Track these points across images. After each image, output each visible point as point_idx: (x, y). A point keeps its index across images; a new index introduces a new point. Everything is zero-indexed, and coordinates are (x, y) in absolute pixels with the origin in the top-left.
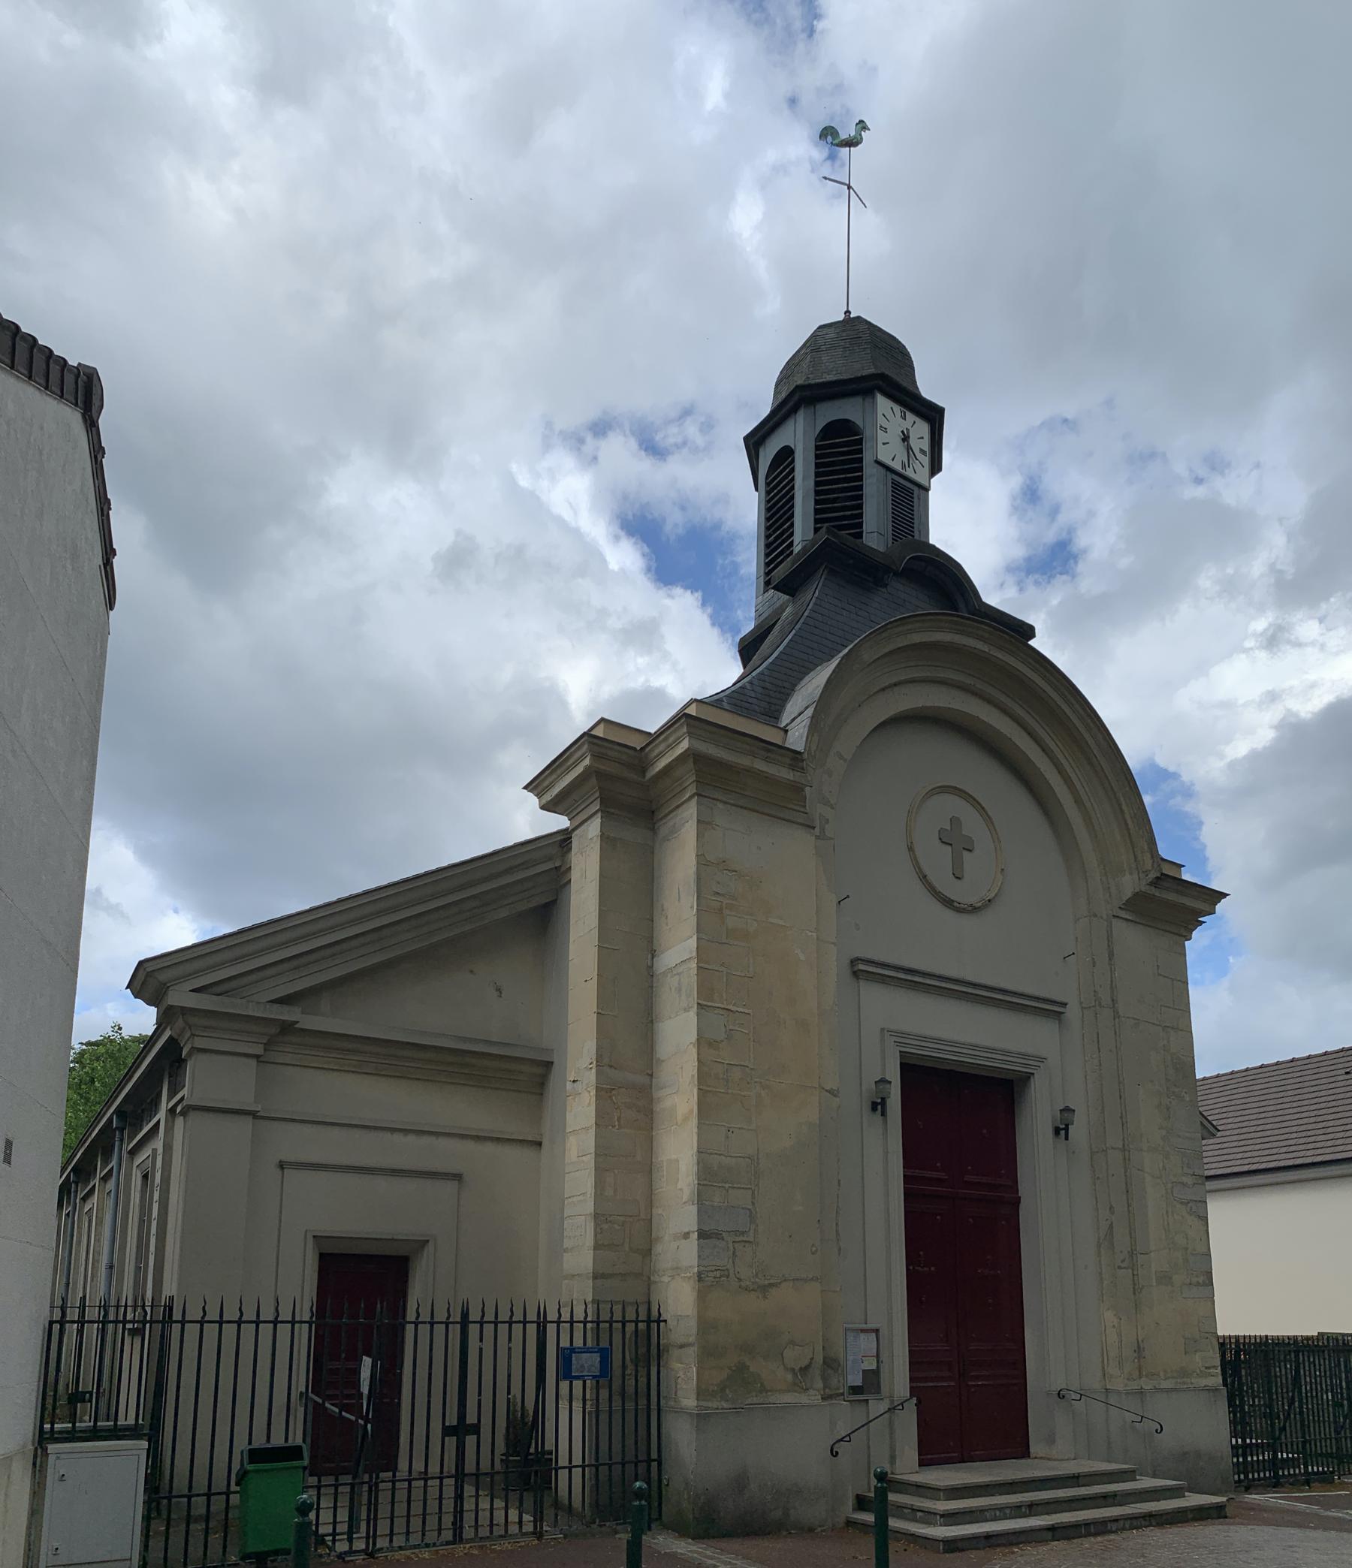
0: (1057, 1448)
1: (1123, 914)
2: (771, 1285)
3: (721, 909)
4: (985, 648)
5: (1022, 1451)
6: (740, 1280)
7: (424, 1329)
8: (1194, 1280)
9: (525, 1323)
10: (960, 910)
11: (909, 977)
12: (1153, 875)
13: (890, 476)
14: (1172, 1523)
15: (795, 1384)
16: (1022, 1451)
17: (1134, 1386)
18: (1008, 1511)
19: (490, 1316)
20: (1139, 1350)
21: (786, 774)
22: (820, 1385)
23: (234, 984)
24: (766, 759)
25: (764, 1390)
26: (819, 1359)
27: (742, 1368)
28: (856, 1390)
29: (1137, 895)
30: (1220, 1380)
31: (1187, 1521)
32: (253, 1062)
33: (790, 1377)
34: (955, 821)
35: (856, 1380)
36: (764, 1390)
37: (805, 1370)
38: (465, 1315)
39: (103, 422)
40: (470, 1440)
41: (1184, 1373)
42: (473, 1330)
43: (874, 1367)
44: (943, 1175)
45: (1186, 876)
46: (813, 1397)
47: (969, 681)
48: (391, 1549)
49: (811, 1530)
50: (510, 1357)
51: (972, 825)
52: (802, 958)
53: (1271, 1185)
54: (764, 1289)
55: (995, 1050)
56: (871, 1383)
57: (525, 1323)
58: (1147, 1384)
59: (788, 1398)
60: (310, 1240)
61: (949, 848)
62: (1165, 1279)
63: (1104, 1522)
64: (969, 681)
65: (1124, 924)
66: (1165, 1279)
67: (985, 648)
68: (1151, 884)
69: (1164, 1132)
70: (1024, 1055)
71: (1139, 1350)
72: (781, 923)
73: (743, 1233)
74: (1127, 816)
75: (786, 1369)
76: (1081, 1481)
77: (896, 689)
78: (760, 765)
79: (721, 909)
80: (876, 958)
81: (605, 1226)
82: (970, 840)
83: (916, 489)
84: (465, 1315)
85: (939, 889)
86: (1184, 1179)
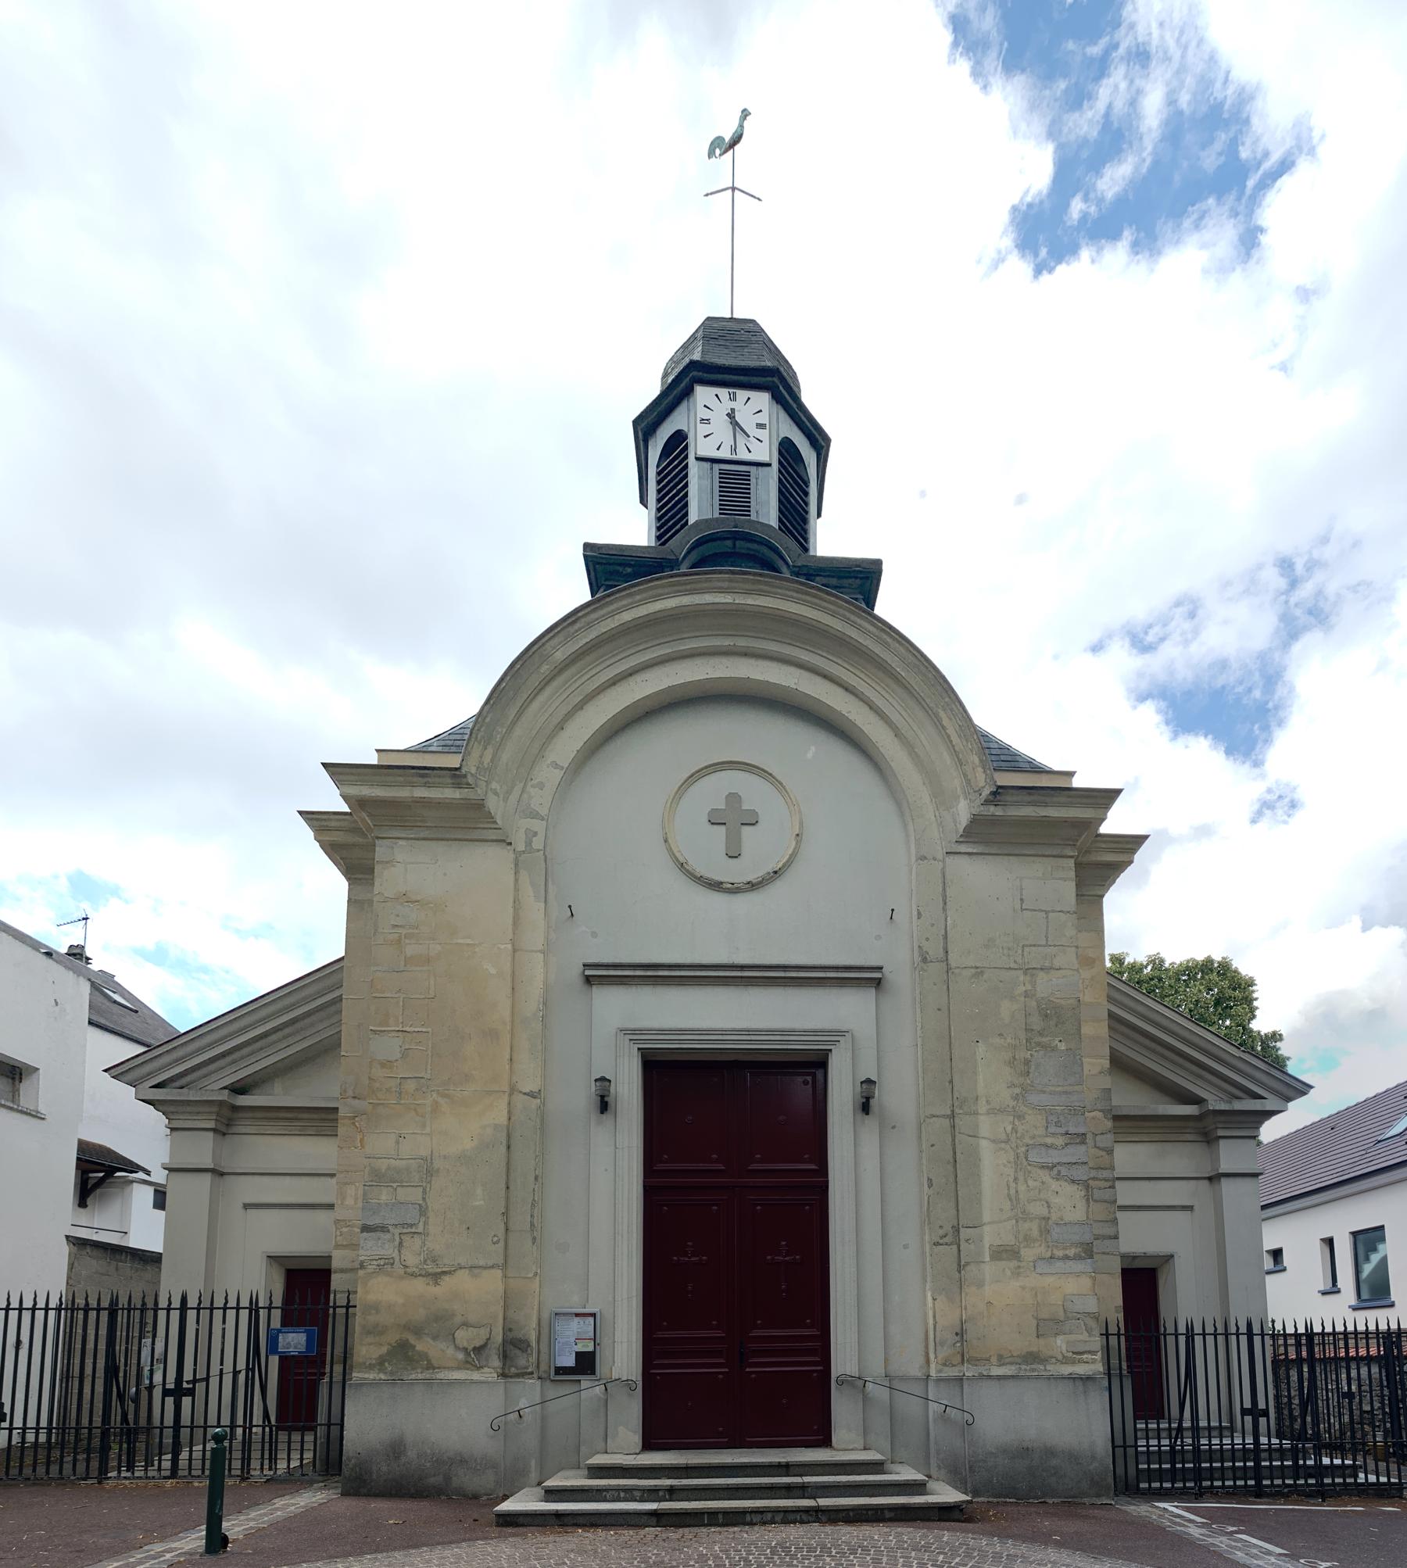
0: (850, 1437)
1: (963, 848)
2: (444, 1273)
3: (399, 941)
4: (727, 599)
5: (826, 1442)
8: (1060, 1253)
9: (238, 1308)
12: (986, 792)
13: (717, 467)
16: (826, 1442)
17: (952, 1372)
19: (232, 1303)
20: (961, 1334)
21: (450, 794)
23: (188, 1079)
24: (426, 785)
25: (430, 1367)
28: (560, 1371)
29: (975, 821)
30: (1100, 1367)
31: (929, 1520)
32: (211, 1134)
33: (461, 1356)
34: (733, 799)
37: (478, 1350)
38: (184, 1300)
39: (1056, 769)
40: (186, 1401)
41: (1032, 1358)
42: (191, 1315)
43: (590, 1349)
45: (1077, 782)
46: (489, 1374)
47: (727, 642)
48: (119, 1477)
49: (475, 1497)
50: (223, 1337)
51: (753, 792)
52: (493, 971)
54: (436, 1277)
56: (586, 1363)
58: (969, 1371)
61: (723, 828)
62: (1002, 1253)
64: (727, 642)
65: (965, 860)
66: (1002, 1253)
67: (727, 599)
68: (987, 802)
69: (1018, 1090)
71: (961, 1334)
72: (469, 941)
73: (411, 1226)
74: (951, 731)
75: (457, 1348)
77: (631, 679)
79: (399, 941)
80: (617, 961)
81: (345, 1230)
82: (754, 813)
83: (753, 469)
84: (184, 1300)
85: (707, 874)
86: (1049, 1141)
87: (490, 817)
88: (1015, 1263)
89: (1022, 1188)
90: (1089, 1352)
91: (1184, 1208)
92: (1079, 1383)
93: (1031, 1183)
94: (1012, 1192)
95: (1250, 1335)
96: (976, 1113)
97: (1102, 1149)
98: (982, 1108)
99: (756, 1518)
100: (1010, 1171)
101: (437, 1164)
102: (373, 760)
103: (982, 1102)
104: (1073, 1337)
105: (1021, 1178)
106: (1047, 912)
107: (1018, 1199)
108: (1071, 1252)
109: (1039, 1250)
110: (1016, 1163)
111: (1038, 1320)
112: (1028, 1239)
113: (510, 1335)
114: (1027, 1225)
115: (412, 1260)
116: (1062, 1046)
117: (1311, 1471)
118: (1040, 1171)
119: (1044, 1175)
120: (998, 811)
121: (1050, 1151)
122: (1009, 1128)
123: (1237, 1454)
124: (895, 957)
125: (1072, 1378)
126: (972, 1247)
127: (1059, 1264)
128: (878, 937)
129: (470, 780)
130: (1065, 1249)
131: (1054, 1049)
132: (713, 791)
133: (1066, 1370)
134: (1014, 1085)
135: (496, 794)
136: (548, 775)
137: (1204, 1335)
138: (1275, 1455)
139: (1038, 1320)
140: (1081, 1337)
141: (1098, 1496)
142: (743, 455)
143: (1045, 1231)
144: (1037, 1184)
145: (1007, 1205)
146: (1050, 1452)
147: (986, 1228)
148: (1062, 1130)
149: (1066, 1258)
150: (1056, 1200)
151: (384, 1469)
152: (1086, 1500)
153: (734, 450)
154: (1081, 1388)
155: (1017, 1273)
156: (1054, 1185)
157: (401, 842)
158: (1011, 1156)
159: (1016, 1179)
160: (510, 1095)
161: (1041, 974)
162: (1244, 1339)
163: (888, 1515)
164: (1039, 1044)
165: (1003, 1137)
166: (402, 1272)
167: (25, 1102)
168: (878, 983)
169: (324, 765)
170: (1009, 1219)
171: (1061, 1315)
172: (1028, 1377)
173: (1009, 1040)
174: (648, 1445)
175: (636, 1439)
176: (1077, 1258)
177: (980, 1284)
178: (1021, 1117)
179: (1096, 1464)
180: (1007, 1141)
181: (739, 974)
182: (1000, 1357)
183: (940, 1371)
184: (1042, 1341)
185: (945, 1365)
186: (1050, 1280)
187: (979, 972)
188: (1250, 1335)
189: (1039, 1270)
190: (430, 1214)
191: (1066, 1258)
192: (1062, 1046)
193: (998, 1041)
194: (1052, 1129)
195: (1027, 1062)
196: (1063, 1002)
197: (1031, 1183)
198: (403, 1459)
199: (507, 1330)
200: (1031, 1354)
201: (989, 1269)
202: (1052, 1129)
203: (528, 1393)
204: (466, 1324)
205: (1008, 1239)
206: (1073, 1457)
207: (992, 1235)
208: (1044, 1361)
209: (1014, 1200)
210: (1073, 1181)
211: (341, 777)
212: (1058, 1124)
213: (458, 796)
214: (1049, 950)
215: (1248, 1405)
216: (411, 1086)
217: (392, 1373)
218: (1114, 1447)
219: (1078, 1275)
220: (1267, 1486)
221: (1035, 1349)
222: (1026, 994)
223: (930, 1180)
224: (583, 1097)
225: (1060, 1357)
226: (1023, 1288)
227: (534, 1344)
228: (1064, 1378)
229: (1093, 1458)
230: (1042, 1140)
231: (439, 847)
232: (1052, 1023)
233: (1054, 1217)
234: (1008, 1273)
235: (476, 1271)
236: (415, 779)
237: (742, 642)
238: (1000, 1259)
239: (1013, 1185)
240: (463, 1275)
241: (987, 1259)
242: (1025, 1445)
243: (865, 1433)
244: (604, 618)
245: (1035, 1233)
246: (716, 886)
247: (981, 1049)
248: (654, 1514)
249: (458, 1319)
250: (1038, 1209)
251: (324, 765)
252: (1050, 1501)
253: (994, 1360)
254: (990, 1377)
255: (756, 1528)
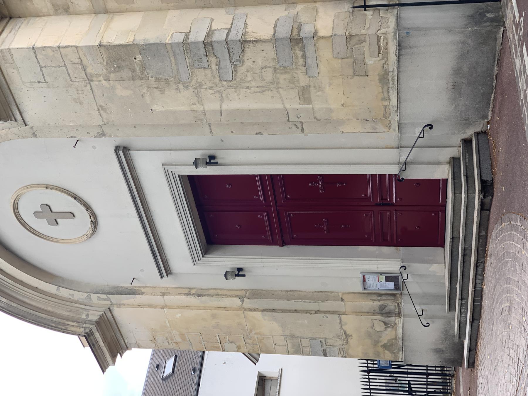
1: (19, 117)
6: (343, 344)
8: (301, 61)
11: (158, 254)
15: (393, 327)
21: (97, 335)
24: (97, 342)
25: (396, 339)
26: (380, 318)
27: (385, 346)
28: (397, 287)
33: (389, 329)
35: (391, 285)
36: (396, 339)
37: (385, 324)
41: (384, 79)
44: (265, 214)
46: (399, 322)
52: (180, 315)
53: (232, 290)
54: (347, 336)
55: (176, 204)
59: (400, 331)
66: (304, 95)
69: (181, 86)
78: (101, 343)
86: (214, 67)
87: (101, 317)
88: (312, 89)
89: (253, 84)
90: (378, 41)
92: (403, 52)
93: (249, 79)
96: (204, 111)
98: (199, 108)
100: (243, 91)
101: (287, 333)
102: (89, 349)
103: (194, 107)
104: (367, 53)
105: (246, 85)
106: (41, 67)
108: (299, 53)
110: (236, 88)
112: (293, 81)
114: (282, 81)
116: (139, 57)
118: (239, 74)
119: (242, 70)
121: (222, 66)
122: (211, 91)
124: (106, 148)
125: (399, 55)
126: (302, 115)
127: (309, 61)
128: (94, 147)
130: (297, 57)
131: (143, 63)
133: (393, 57)
134: (178, 89)
135: (88, 315)
141: (496, 39)
144: (249, 74)
145: (269, 93)
146: (457, 71)
147: (288, 106)
148: (205, 58)
149: (304, 56)
150: (260, 63)
151: (448, 354)
152: (498, 48)
154: (407, 50)
155: (320, 88)
156: (248, 63)
157: (126, 341)
158: (230, 90)
159: (248, 88)
160: (245, 310)
161: (89, 70)
163: (483, 233)
164: (142, 72)
165: (217, 95)
166: (346, 346)
168: (126, 149)
169: (103, 372)
170: (279, 93)
172: (398, 85)
173: (145, 91)
174: (443, 245)
175: (440, 249)
176: (303, 49)
177: (330, 111)
179: (469, 41)
180: (221, 94)
181: (159, 258)
182: (383, 99)
184: (370, 73)
185: (390, 128)
187: (100, 108)
189: (316, 74)
190: (314, 337)
191: (304, 56)
192: (139, 57)
193: (147, 98)
195: (158, 80)
196: (105, 56)
197: (249, 79)
198: (444, 349)
199: (374, 313)
200: (380, 81)
201: (318, 105)
203: (407, 307)
204: (372, 327)
205: (294, 93)
206: (462, 56)
207: (292, 103)
209: (263, 89)
210: (243, 51)
211: (106, 365)
212: (200, 61)
213: (97, 333)
214: (69, 66)
216: (249, 341)
217: (399, 350)
219: (316, 49)
221: (377, 78)
222: (107, 79)
223: (257, 134)
224: (238, 283)
226: (330, 84)
227: (382, 303)
228: (399, 62)
229: (464, 43)
230: (215, 72)
231: (123, 330)
232: (123, 63)
233: (273, 64)
234: (319, 93)
235: (343, 323)
236: (96, 347)
238: (310, 99)
239: (253, 90)
241: (311, 106)
242: (450, 86)
245: (287, 76)
246: (88, 208)
247: (157, 108)
248: (472, 322)
249: (370, 330)
250: (269, 75)
251: (103, 372)
252: (496, 72)
253: (386, 103)
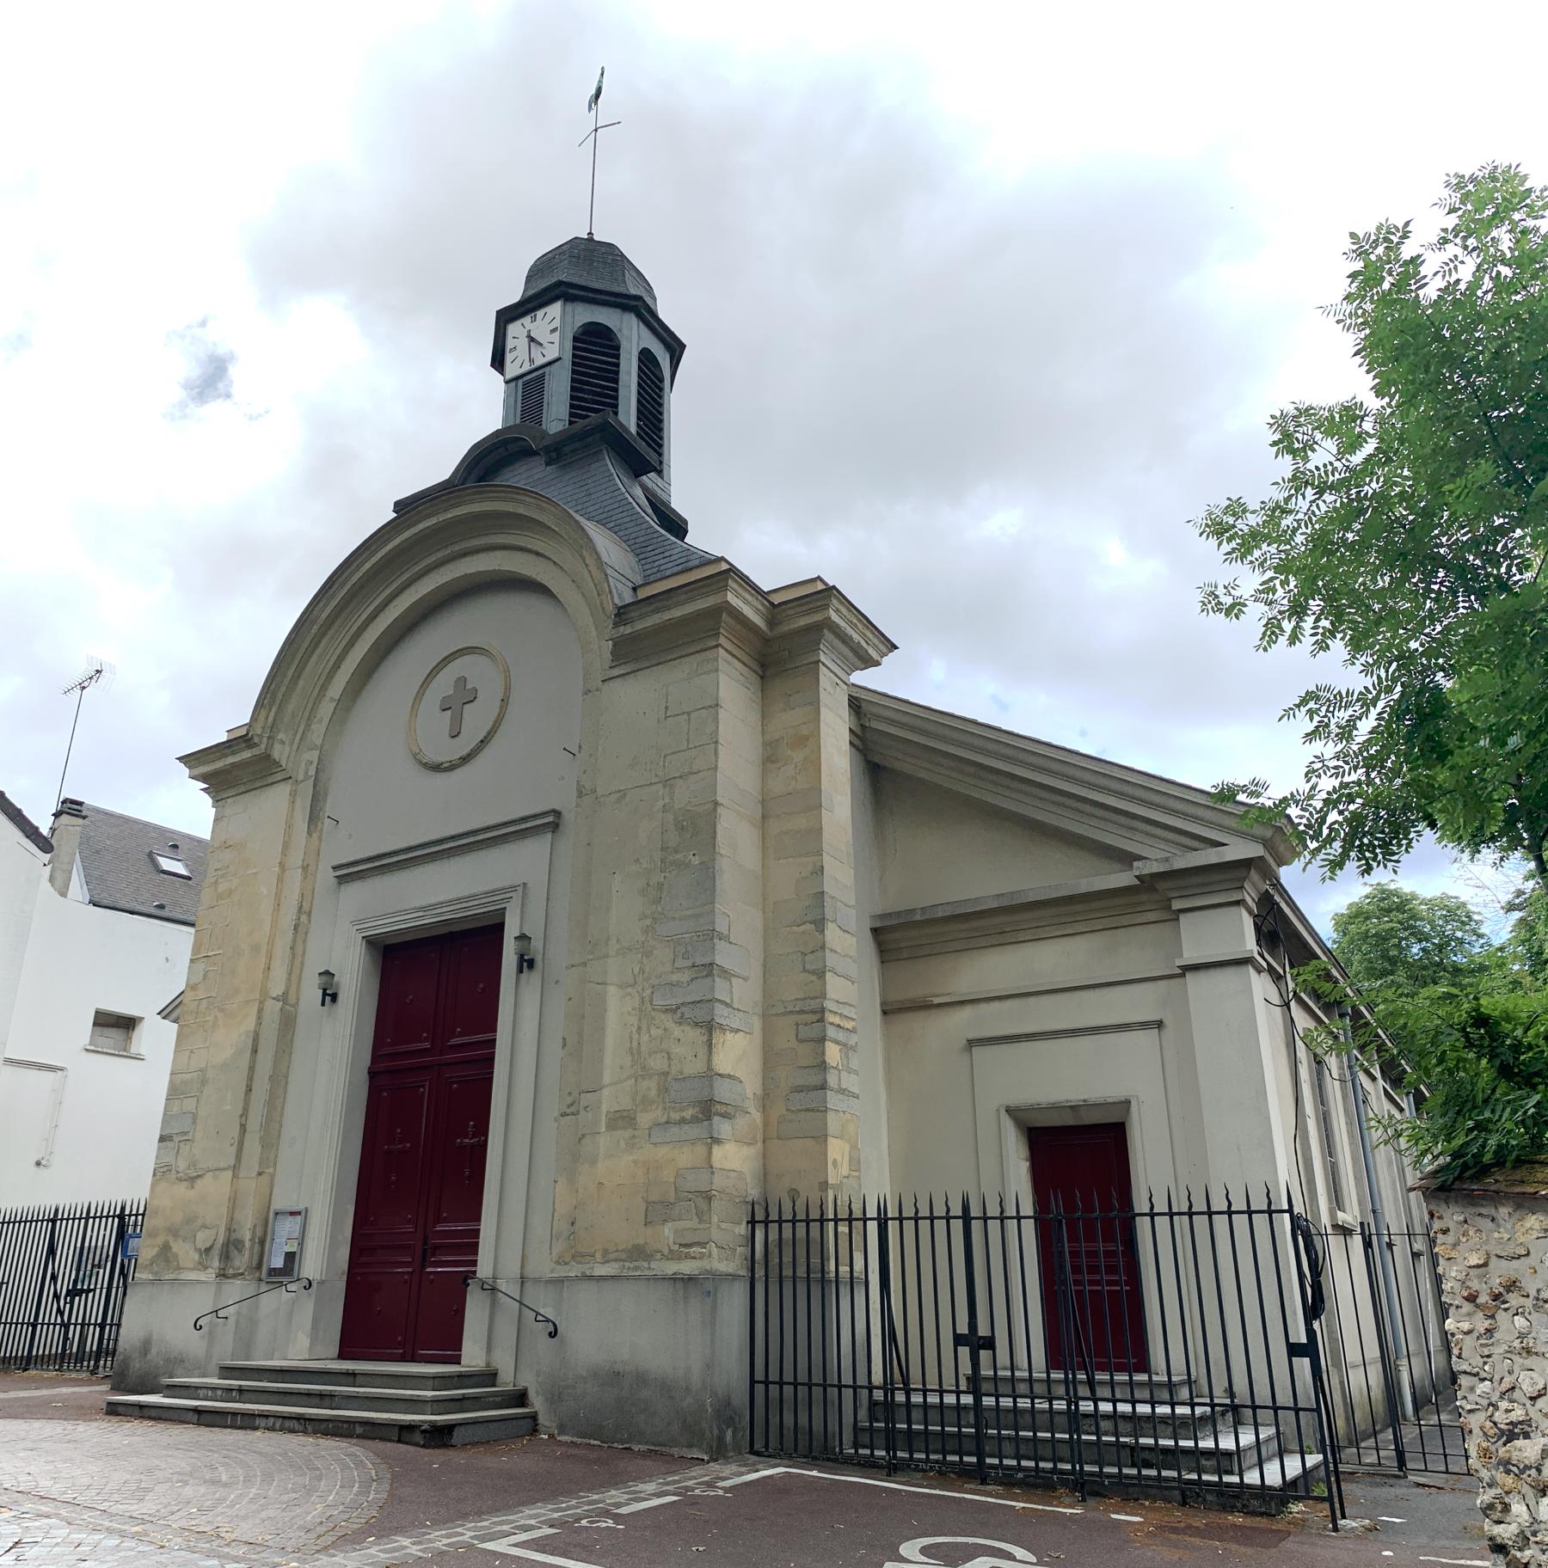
1: (616, 672)
4: (433, 521)
7: (994, 1226)
8: (676, 1116)
10: (452, 767)
14: (326, 1434)
16: (456, 1360)
18: (219, 1393)
22: (216, 1264)
24: (233, 753)
25: (178, 1268)
27: (166, 1247)
28: (273, 1272)
33: (197, 1257)
34: (462, 681)
36: (178, 1268)
37: (208, 1250)
38: (966, 1208)
41: (639, 1253)
46: (209, 1276)
54: (192, 1180)
57: (1019, 1218)
59: (192, 1276)
60: (1003, 1114)
63: (253, 1415)
66: (622, 1119)
67: (433, 521)
69: (648, 922)
70: (493, 892)
73: (186, 1133)
76: (359, 1379)
80: (344, 861)
84: (966, 1208)
86: (675, 978)
87: (277, 764)
90: (698, 1244)
91: (1144, 1025)
92: (679, 1285)
94: (635, 1044)
95: (967, 1218)
97: (813, 972)
99: (218, 1419)
104: (680, 1225)
105: (644, 1027)
107: (639, 1053)
108: (688, 1114)
109: (657, 1114)
111: (648, 1203)
113: (234, 1236)
114: (645, 1083)
115: (182, 1165)
117: (1146, 1455)
118: (663, 1016)
119: (667, 1021)
120: (628, 630)
122: (636, 970)
123: (1057, 1419)
125: (674, 1279)
127: (675, 1129)
129: (256, 740)
130: (682, 1110)
131: (688, 865)
132: (444, 684)
133: (671, 1268)
135: (283, 742)
136: (326, 709)
137: (901, 1219)
138: (1122, 1426)
139: (648, 1203)
140: (689, 1224)
141: (690, 1446)
142: (540, 361)
143: (664, 1090)
144: (660, 1032)
146: (641, 1379)
147: (606, 1092)
149: (683, 1121)
150: (678, 1050)
152: (675, 1451)
153: (531, 361)
154: (681, 1293)
156: (677, 1031)
159: (639, 1028)
161: (680, 782)
162: (957, 1225)
163: (359, 1430)
165: (631, 981)
167: (133, 1050)
170: (628, 1078)
171: (672, 1197)
172: (627, 1278)
174: (343, 1355)
176: (695, 1120)
177: (593, 1162)
178: (648, 954)
179: (689, 1400)
182: (606, 1252)
183: (552, 1271)
185: (558, 1263)
186: (663, 1151)
188: (967, 1218)
191: (683, 1121)
192: (696, 861)
194: (680, 963)
195: (660, 886)
199: (229, 1230)
202: (680, 963)
204: (204, 1226)
205: (625, 1102)
206: (666, 1387)
207: (609, 1100)
208: (648, 1257)
209: (635, 1053)
210: (696, 1024)
215: (963, 1329)
218: (753, 1382)
220: (992, 1466)
221: (642, 1242)
225: (666, 1252)
226: (635, 1162)
229: (688, 1389)
234: (623, 1145)
237: (457, 548)
239: (635, 1036)
240: (209, 1177)
243: (489, 1349)
244: (353, 573)
245: (653, 1093)
246: (465, 760)
248: (196, 1410)
250: (658, 1063)
253: (598, 1256)
254: (590, 1277)
255: (258, 1433)
